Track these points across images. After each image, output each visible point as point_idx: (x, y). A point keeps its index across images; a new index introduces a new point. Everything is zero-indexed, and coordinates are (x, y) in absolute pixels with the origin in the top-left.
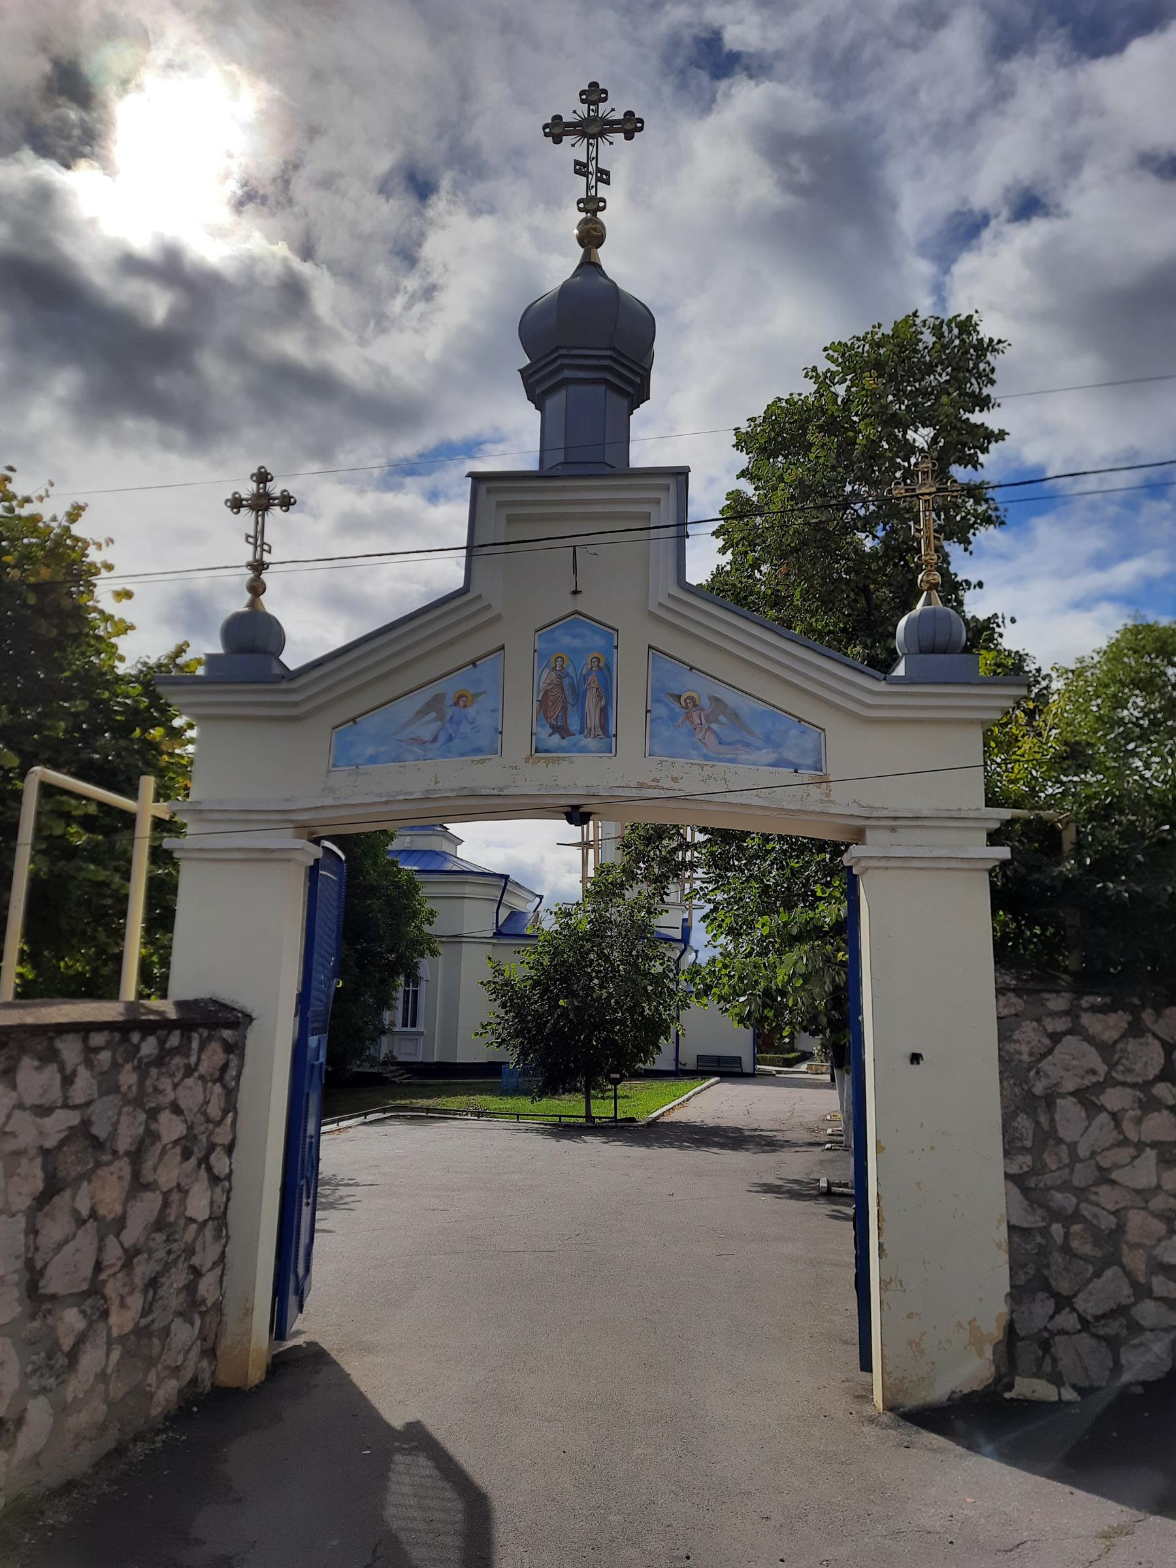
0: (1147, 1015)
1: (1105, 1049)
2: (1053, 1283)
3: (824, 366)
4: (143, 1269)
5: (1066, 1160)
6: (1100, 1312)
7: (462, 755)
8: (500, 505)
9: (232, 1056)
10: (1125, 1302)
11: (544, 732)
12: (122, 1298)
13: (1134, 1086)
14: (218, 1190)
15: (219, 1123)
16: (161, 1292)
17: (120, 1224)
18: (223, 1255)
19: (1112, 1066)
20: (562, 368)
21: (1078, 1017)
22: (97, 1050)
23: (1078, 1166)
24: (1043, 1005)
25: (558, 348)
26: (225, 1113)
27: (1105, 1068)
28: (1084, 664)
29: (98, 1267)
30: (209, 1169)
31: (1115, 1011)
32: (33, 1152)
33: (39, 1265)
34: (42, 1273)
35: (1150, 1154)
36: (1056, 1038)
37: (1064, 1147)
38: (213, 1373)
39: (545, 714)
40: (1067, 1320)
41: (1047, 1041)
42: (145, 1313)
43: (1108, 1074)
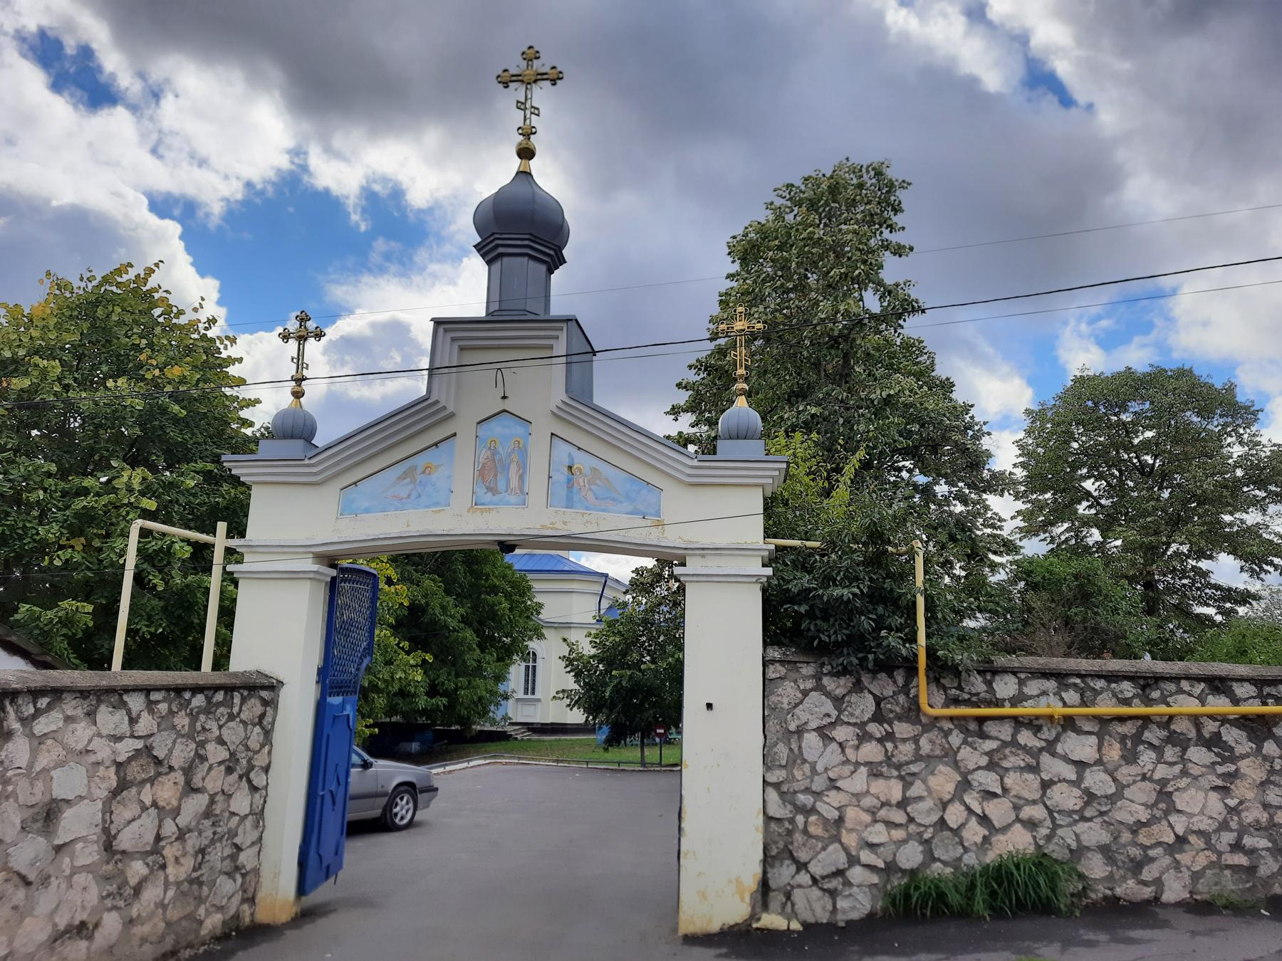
0: (865, 679)
1: (838, 701)
2: (795, 854)
3: (778, 202)
4: (193, 842)
5: (808, 773)
6: (825, 873)
7: (427, 507)
8: (453, 339)
9: (268, 709)
10: (841, 867)
11: (481, 491)
12: (177, 859)
13: (855, 724)
14: (257, 796)
15: (258, 752)
16: (207, 857)
17: (176, 812)
18: (261, 838)
19: (840, 712)
20: (497, 246)
21: (820, 679)
22: (157, 702)
23: (816, 778)
24: (798, 671)
25: (493, 234)
26: (262, 746)
27: (836, 713)
28: (1045, 407)
29: (158, 838)
30: (249, 781)
31: (845, 675)
32: (107, 763)
33: (113, 832)
34: (115, 837)
35: (863, 770)
36: (805, 693)
37: (807, 765)
38: (252, 915)
39: (483, 479)
40: (804, 878)
41: (800, 695)
42: (195, 870)
43: (838, 717)
